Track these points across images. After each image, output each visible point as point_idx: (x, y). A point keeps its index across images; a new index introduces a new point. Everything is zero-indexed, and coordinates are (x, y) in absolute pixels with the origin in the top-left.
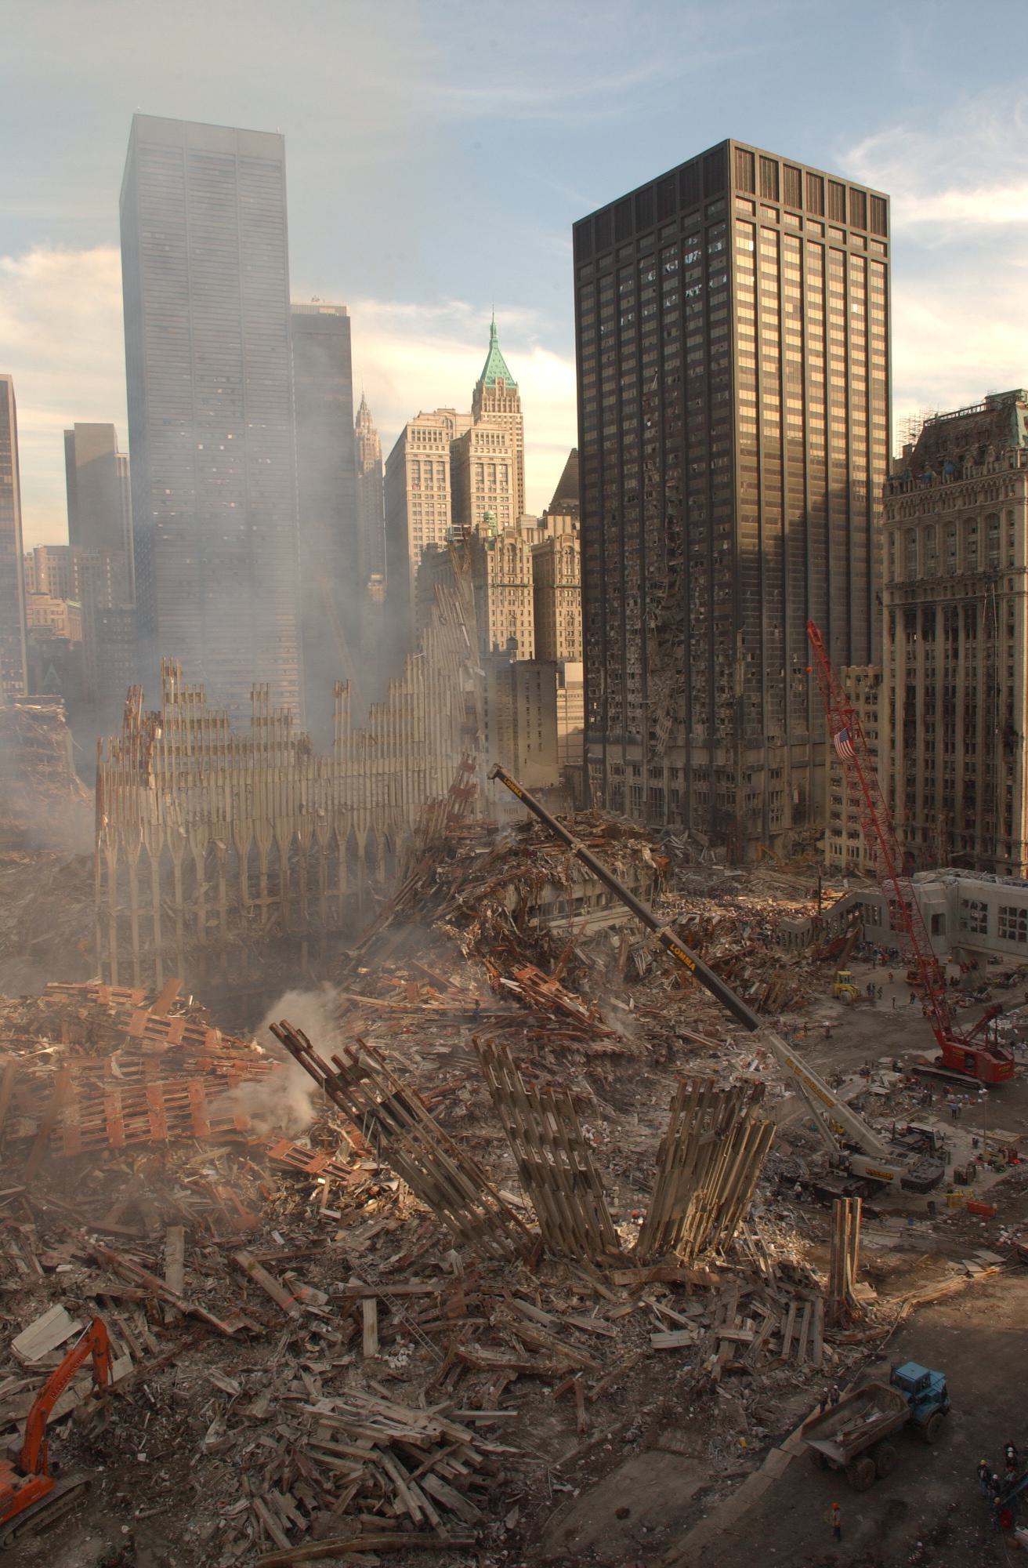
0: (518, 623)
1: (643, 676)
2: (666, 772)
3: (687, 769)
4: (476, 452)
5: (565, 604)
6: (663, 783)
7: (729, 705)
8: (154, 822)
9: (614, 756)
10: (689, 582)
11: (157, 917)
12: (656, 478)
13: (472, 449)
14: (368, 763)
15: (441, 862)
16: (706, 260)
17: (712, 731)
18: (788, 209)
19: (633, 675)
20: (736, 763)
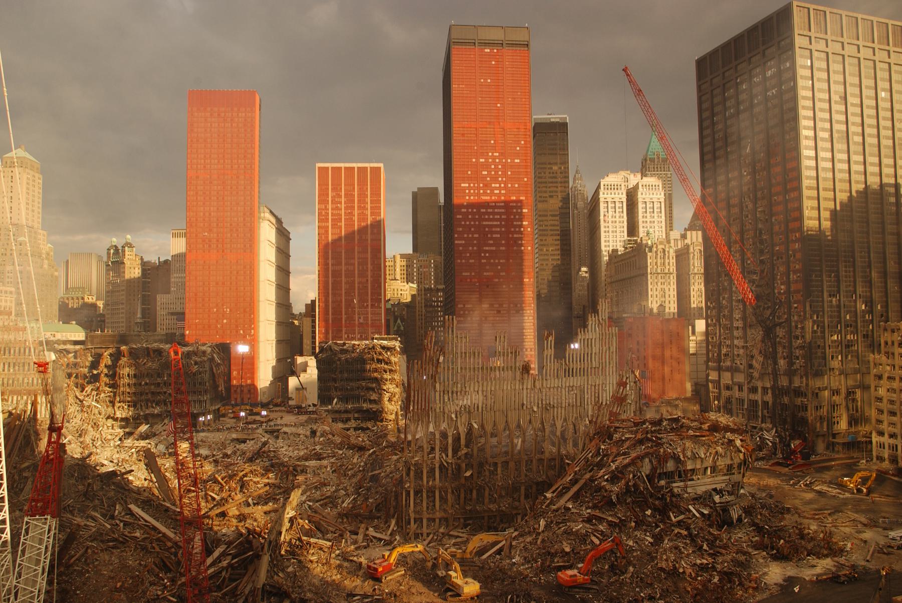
0: (667, 296)
1: (744, 329)
2: (760, 390)
3: (773, 388)
4: (641, 197)
5: (696, 284)
6: (758, 397)
7: (801, 347)
8: (438, 410)
9: (726, 378)
10: (774, 270)
11: (437, 466)
12: (750, 206)
13: (639, 193)
14: (564, 379)
15: (604, 442)
16: (780, 73)
17: (791, 364)
18: (834, 38)
19: (737, 328)
20: (807, 385)
